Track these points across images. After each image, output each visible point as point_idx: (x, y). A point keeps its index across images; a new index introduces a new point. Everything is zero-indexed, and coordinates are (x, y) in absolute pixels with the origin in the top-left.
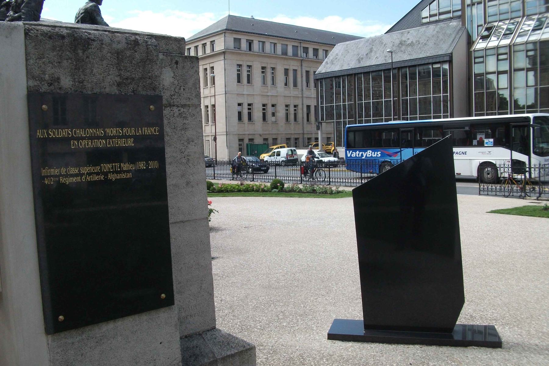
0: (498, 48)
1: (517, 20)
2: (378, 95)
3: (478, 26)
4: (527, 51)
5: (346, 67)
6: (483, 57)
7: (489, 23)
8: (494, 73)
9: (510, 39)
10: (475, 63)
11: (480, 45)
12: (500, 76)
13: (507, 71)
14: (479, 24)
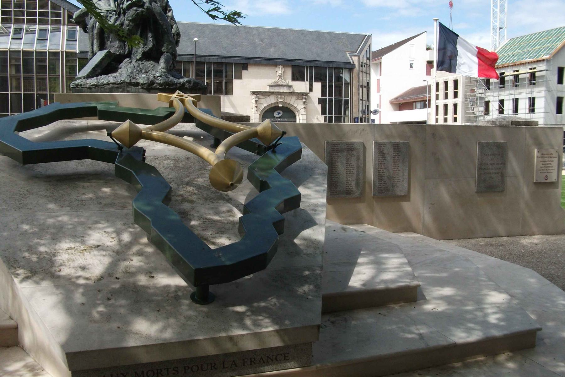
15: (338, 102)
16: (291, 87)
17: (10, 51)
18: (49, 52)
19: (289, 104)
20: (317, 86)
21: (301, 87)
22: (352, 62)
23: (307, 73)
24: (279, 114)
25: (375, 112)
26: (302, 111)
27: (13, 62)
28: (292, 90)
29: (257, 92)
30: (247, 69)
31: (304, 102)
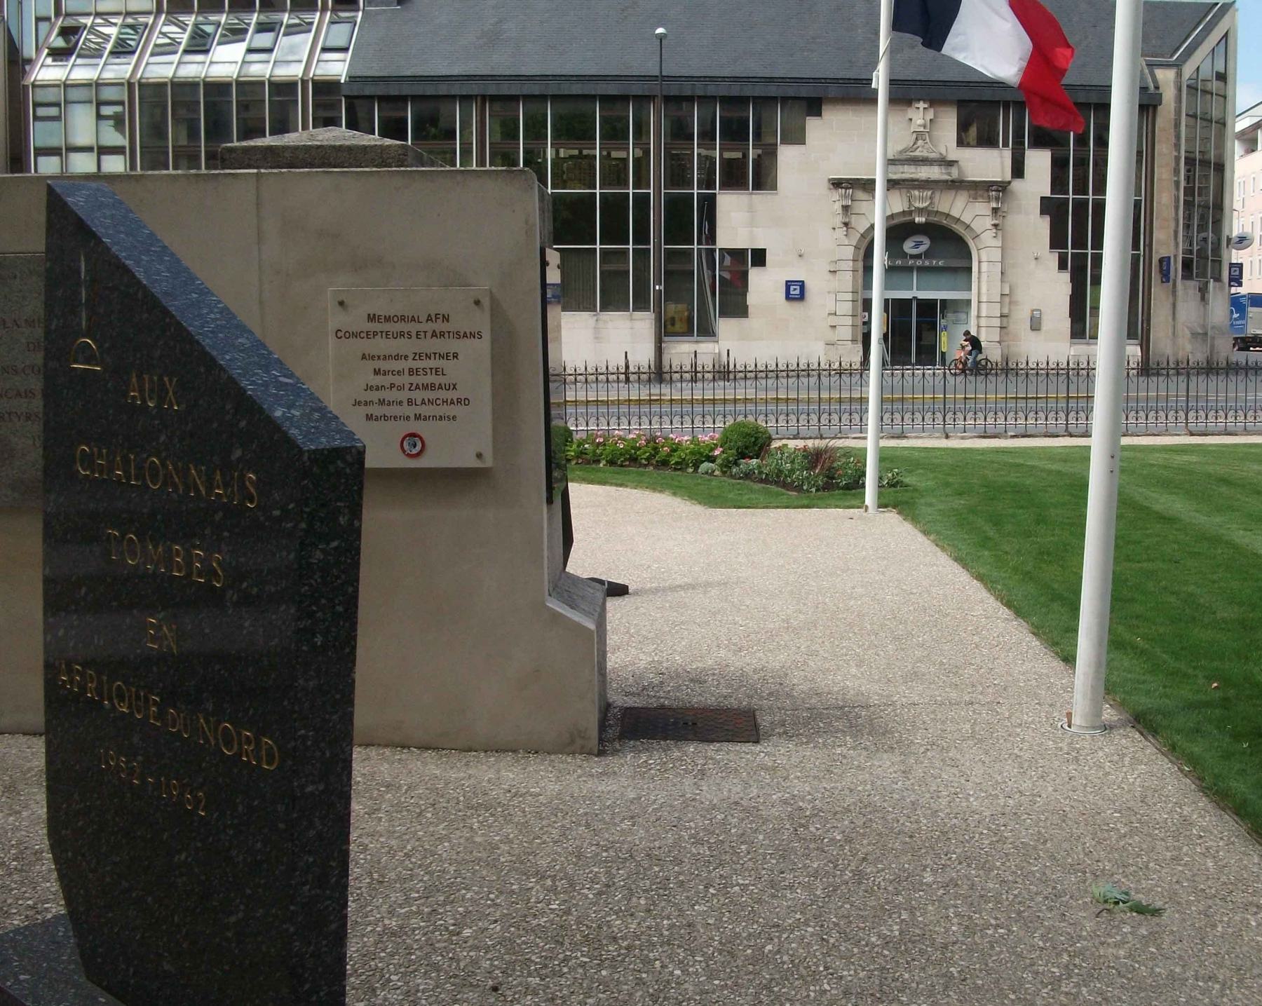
0: (98, 85)
1: (142, 19)
2: (615, 174)
3: (38, 19)
4: (100, 104)
5: (531, 68)
6: (58, 105)
7: (67, 15)
8: (88, 149)
9: (131, 68)
10: (36, 118)
11: (47, 72)
12: (104, 158)
13: (124, 147)
14: (43, 13)
15: (1081, 207)
16: (951, 163)
17: (271, 83)
18: (271, 83)
19: (948, 215)
20: (1039, 162)
21: (988, 163)
22: (1152, 86)
23: (1004, 124)
24: (917, 245)
25: (1243, 241)
26: (988, 238)
27: (182, 112)
28: (955, 173)
29: (848, 180)
30: (819, 114)
31: (995, 210)
